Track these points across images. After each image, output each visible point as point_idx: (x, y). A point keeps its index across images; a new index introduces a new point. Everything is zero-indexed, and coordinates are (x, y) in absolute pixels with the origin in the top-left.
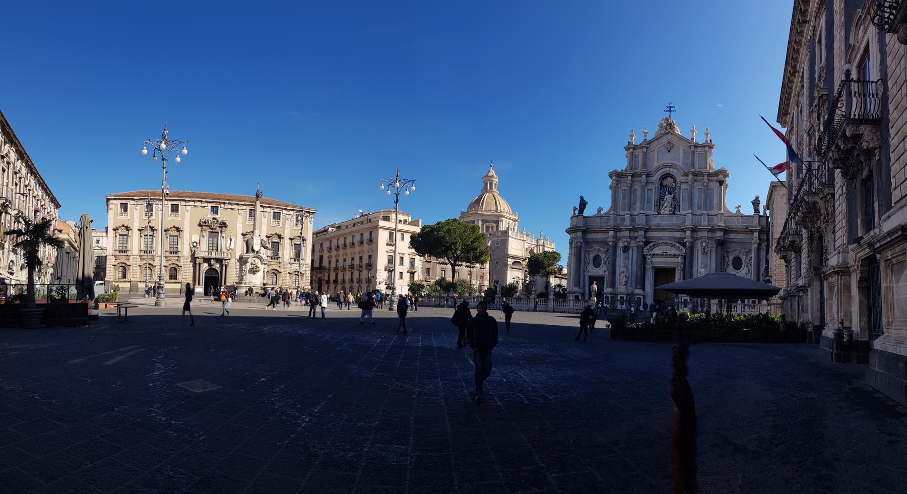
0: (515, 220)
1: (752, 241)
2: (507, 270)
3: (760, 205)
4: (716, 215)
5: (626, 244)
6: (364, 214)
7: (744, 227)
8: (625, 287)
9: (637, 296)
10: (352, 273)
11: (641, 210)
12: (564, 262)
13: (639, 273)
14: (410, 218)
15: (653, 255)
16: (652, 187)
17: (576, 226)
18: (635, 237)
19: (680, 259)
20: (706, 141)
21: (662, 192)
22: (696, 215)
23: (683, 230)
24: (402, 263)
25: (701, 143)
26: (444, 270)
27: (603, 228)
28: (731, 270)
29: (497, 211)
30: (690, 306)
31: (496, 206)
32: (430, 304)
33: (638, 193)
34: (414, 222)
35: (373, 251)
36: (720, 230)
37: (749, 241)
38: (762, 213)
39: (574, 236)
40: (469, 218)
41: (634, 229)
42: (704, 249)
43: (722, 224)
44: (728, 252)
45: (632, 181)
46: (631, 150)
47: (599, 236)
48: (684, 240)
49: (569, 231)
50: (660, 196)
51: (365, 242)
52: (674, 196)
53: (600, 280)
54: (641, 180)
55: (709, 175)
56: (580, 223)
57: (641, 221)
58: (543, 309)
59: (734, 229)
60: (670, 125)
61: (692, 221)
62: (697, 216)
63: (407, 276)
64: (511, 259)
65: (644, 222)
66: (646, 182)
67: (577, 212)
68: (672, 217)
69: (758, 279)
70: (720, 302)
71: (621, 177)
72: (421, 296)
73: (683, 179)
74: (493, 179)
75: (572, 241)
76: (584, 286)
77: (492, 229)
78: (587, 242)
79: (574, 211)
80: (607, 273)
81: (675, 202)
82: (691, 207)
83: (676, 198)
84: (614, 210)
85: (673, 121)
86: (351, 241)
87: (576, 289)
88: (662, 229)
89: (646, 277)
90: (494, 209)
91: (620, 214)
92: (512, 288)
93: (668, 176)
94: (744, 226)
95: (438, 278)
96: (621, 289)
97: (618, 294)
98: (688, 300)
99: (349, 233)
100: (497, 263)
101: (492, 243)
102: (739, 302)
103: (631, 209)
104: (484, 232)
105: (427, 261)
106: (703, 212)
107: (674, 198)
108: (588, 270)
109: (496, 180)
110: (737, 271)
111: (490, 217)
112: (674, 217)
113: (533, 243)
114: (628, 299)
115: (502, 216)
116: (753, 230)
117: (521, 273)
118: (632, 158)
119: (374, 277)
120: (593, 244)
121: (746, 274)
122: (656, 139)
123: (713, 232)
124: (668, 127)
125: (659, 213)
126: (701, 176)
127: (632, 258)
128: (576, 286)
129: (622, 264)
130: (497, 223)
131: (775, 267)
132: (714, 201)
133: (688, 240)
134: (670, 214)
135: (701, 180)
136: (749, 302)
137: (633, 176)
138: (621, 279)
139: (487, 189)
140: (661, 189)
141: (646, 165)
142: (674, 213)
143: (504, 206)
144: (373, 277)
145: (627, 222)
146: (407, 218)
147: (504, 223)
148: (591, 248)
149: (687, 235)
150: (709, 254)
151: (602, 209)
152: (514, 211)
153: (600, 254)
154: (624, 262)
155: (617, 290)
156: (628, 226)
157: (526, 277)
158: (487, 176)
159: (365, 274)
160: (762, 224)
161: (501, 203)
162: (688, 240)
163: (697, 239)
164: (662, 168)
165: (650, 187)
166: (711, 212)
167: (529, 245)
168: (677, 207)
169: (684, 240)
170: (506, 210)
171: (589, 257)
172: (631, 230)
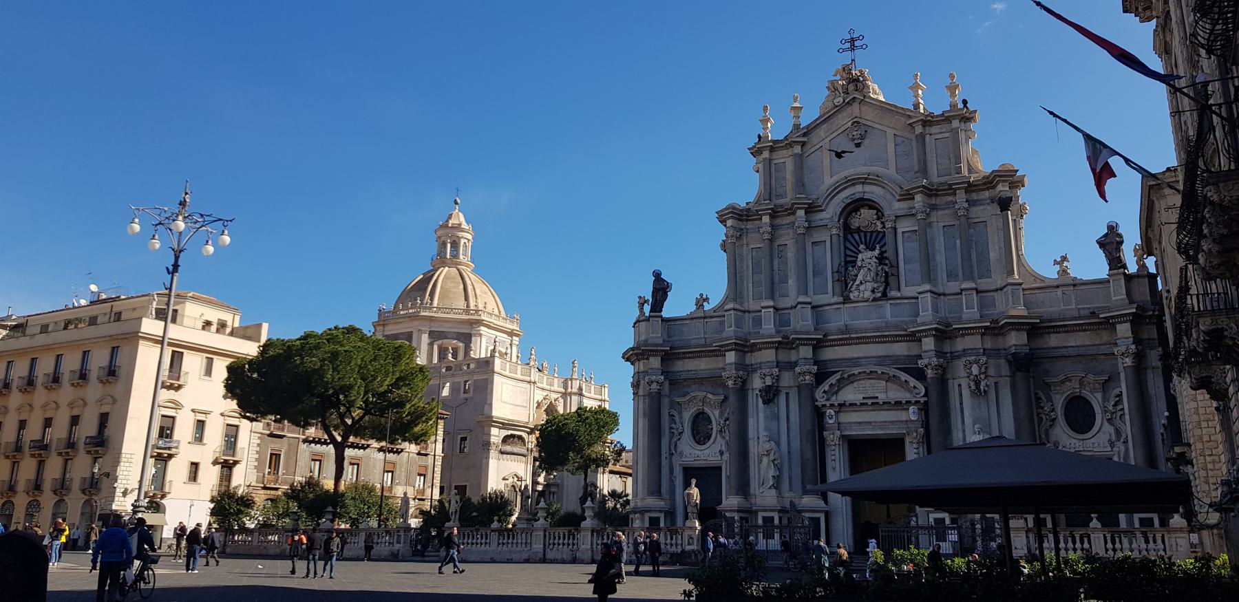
0: (511, 334)
1: (1115, 350)
2: (488, 458)
3: (1124, 247)
4: (1001, 289)
5: (769, 382)
6: (104, 296)
7: (1087, 313)
8: (773, 492)
9: (807, 515)
10: (41, 463)
11: (799, 294)
12: (624, 435)
13: (809, 455)
14: (237, 318)
15: (840, 405)
16: (823, 236)
17: (646, 343)
18: (791, 363)
19: (912, 414)
20: (953, 106)
21: (848, 245)
22: (944, 295)
23: (915, 337)
24: (199, 437)
25: (938, 112)
26: (319, 459)
27: (711, 345)
28: (1065, 438)
29: (467, 310)
30: (953, 536)
31: (467, 298)
32: (264, 552)
33: (791, 254)
34: (246, 328)
35: (115, 401)
36: (1017, 326)
37: (1104, 349)
38: (1132, 268)
39: (642, 369)
40: (399, 326)
41: (786, 344)
42: (977, 383)
43: (1020, 310)
44: (1048, 385)
45: (772, 226)
46: (766, 154)
47: (702, 365)
48: (919, 362)
49: (632, 356)
50: (846, 255)
51: (94, 375)
52: (882, 253)
53: (707, 476)
54: (794, 223)
55: (970, 187)
56: (656, 335)
57: (802, 322)
58: (565, 557)
59: (1056, 320)
60: (856, 83)
61: (936, 310)
62: (946, 298)
63: (210, 477)
64: (500, 428)
65: (809, 324)
66: (806, 225)
67: (647, 308)
68: (880, 307)
69: (1151, 461)
70: (1039, 523)
71: (747, 220)
72: (243, 530)
73: (900, 207)
74: (461, 234)
75: (638, 382)
77: (455, 355)
78: (675, 382)
79: (641, 305)
80: (726, 456)
81: (886, 268)
82: (929, 275)
83: (886, 258)
84: (735, 300)
85: (861, 71)
86: (51, 370)
87: (652, 502)
88: (857, 338)
89: (829, 464)
90: (461, 304)
91: (751, 308)
92: (497, 506)
93: (863, 206)
94: (1084, 309)
95: (299, 478)
96: (765, 497)
97: (756, 512)
98: (948, 522)
99: (47, 348)
100: (464, 439)
101: (453, 389)
102: (1095, 523)
103: (777, 294)
104: (435, 360)
105: (272, 435)
106: (963, 286)
107: (881, 259)
108: (679, 450)
109: (466, 237)
110: (1080, 436)
111: (449, 325)
112: (887, 305)
113: (556, 388)
114: (785, 522)
115: (480, 323)
116: (1112, 317)
117: (523, 465)
118: (769, 172)
119: (111, 476)
120: (690, 386)
121: (1112, 444)
122: (825, 119)
123: (997, 335)
124: (851, 87)
125: (847, 300)
126: (949, 195)
127: (788, 416)
128: (651, 494)
129: (763, 433)
130: (467, 339)
131: (1196, 418)
132: (992, 254)
133: (929, 361)
134: (875, 300)
135: (948, 203)
136: (1130, 522)
137: (774, 214)
138: (762, 471)
139: (445, 258)
140: (846, 239)
141: (803, 185)
142: (884, 294)
143: (485, 299)
144: (108, 475)
145: (768, 327)
146: (227, 317)
147: (484, 339)
148: (685, 396)
149: (925, 348)
150: (992, 395)
151: (707, 300)
152: (510, 308)
153: (707, 410)
154: (767, 429)
155: (753, 501)
156: (772, 337)
157: (535, 474)
158: (445, 226)
159: (81, 467)
160: (1137, 298)
161: (478, 292)
162: (929, 361)
163: (955, 356)
164: (845, 188)
165: (819, 236)
166: (984, 283)
167: (545, 393)
168: (892, 280)
169: (919, 362)
170: (489, 309)
171: (681, 417)
172: (779, 346)
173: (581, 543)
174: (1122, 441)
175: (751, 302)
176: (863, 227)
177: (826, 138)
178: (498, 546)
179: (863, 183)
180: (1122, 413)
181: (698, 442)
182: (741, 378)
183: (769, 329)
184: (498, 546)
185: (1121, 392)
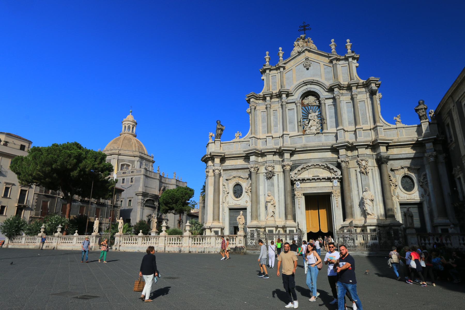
76: (224, 219)
91: (261, 138)
164: (303, 86)
173: (183, 243)
174: (427, 195)
175: (261, 135)
176: (310, 104)
177: (294, 65)
178: (142, 245)
179: (311, 84)
180: (426, 182)
181: (237, 197)
182: (257, 168)
183: (270, 146)
184: (142, 245)
185: (426, 173)
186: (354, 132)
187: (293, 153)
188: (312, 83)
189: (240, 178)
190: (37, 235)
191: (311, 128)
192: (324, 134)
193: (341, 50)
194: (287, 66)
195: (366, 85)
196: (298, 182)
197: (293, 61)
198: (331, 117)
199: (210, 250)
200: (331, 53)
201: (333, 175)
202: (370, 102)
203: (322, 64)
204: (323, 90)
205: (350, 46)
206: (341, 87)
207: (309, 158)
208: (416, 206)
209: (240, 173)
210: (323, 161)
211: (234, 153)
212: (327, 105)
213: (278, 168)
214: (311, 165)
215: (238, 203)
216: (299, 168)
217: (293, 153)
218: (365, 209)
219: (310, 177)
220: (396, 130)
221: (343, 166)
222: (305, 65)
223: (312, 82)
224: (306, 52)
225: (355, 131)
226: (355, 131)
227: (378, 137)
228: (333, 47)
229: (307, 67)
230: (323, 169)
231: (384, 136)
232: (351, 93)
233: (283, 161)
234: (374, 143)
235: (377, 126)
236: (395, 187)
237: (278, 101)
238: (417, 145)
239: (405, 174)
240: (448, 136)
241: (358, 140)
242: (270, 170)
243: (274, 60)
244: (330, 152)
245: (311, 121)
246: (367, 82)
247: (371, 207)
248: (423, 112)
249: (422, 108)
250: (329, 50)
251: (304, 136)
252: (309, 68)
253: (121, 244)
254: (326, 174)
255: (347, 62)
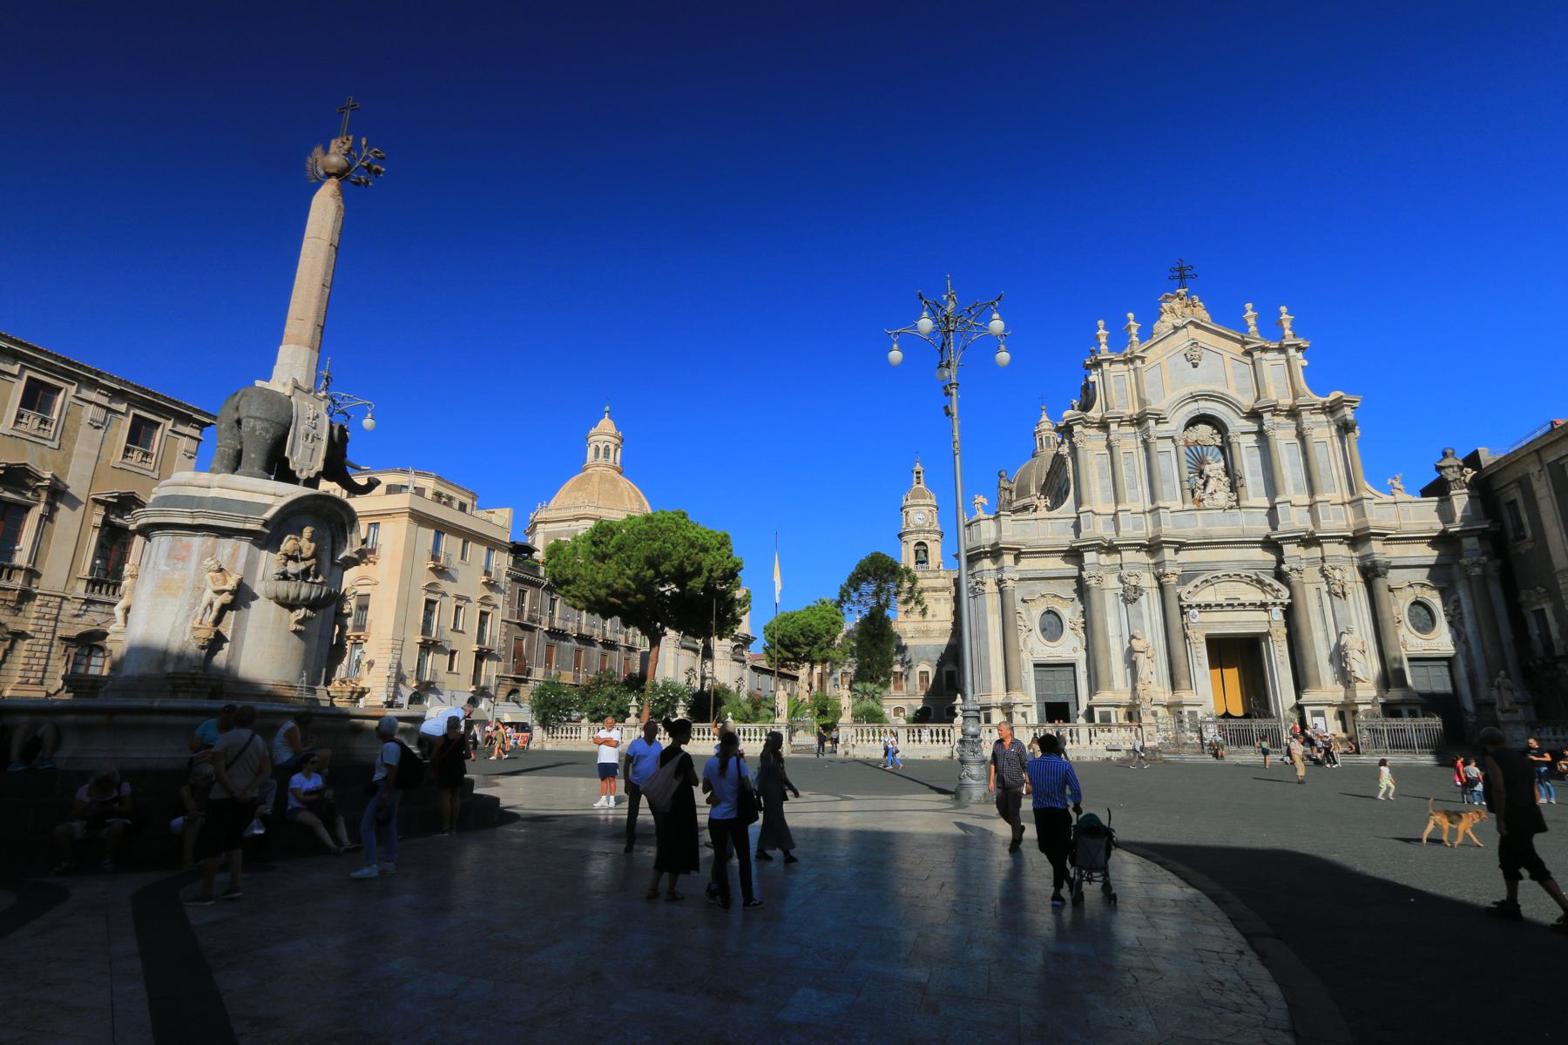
22: (1099, 514)
174: (1462, 641)
179: (1206, 400)
180: (1459, 616)
181: (1050, 639)
183: (1128, 531)
185: (1459, 598)
186: (1307, 508)
187: (1180, 546)
188: (1209, 397)
189: (1056, 599)
190: (624, 721)
191: (1215, 496)
192: (1243, 510)
193: (1271, 327)
194: (1149, 355)
195: (1331, 409)
196: (1196, 611)
197: (1160, 345)
198: (1253, 474)
199: (1081, 755)
200: (1249, 334)
201: (1270, 599)
202: (1340, 445)
203: (1227, 356)
204: (1235, 415)
205: (1105, 338)
206: (1087, 423)
207: (1214, 559)
208: (1445, 663)
209: (1054, 587)
210: (1246, 567)
211: (1040, 543)
212: (1243, 446)
213: (1147, 581)
214: (1224, 575)
215: (1056, 652)
216: (1197, 581)
217: (1019, 554)
218: (1349, 669)
219: (1221, 599)
220: (1394, 506)
221: (1293, 579)
222: (1189, 356)
223: (1210, 396)
224: (1191, 327)
225: (1115, 514)
226: (1115, 514)
227: (1000, 538)
228: (1251, 322)
229: (1194, 361)
230: (1248, 584)
231: (1375, 518)
232: (1108, 436)
233: (1157, 565)
234: (1357, 534)
235: (1158, 508)
236: (1028, 634)
237: (1135, 433)
238: (1441, 541)
239: (1417, 597)
240: (1509, 523)
241: (1121, 534)
242: (1132, 584)
243: (1119, 340)
244: (1261, 547)
245: (1211, 481)
246: (1333, 404)
247: (1362, 666)
248: (1454, 472)
249: (1452, 464)
250: (1244, 327)
251: (1200, 512)
252: (1197, 364)
253: (854, 743)
254: (1256, 595)
255: (1283, 356)
